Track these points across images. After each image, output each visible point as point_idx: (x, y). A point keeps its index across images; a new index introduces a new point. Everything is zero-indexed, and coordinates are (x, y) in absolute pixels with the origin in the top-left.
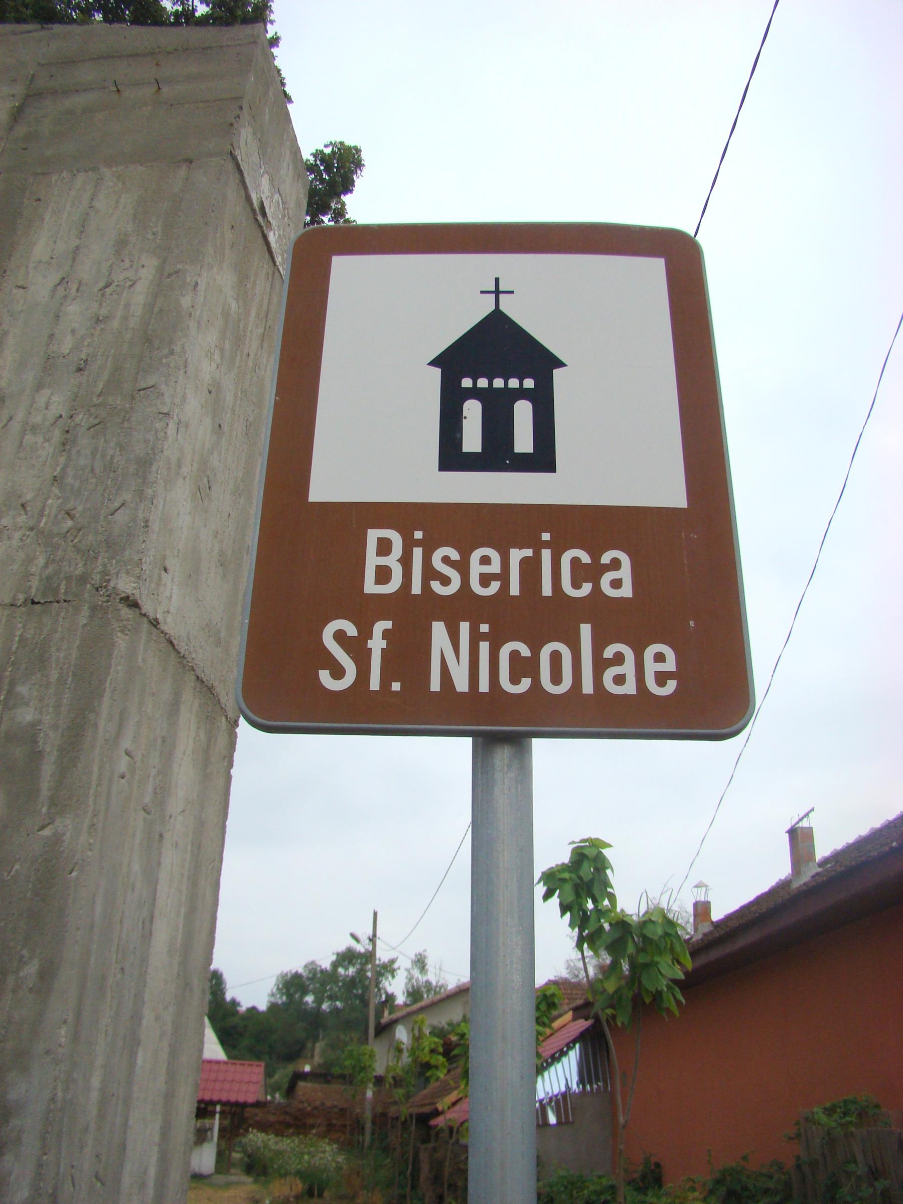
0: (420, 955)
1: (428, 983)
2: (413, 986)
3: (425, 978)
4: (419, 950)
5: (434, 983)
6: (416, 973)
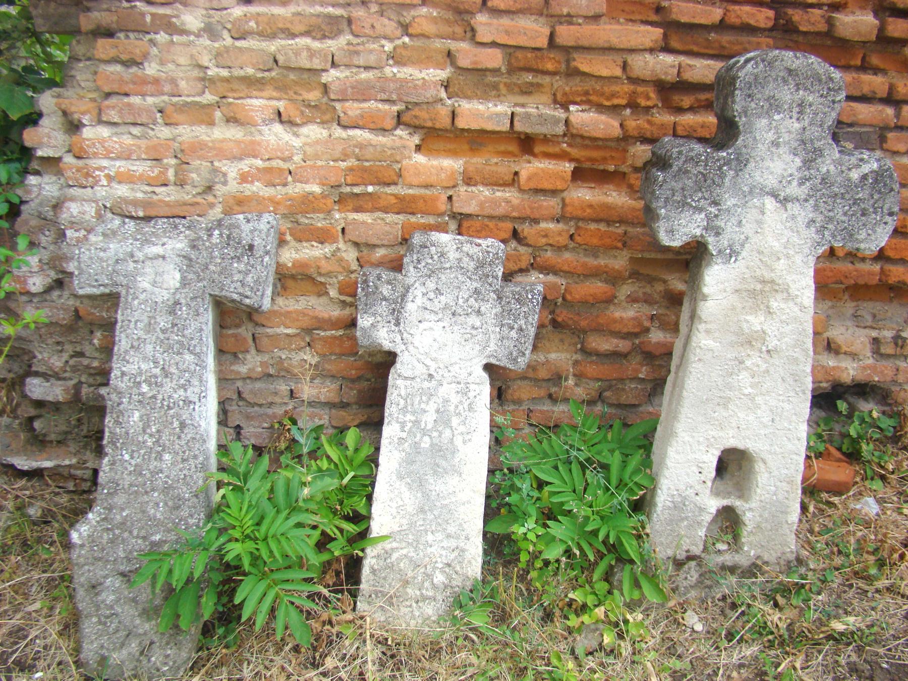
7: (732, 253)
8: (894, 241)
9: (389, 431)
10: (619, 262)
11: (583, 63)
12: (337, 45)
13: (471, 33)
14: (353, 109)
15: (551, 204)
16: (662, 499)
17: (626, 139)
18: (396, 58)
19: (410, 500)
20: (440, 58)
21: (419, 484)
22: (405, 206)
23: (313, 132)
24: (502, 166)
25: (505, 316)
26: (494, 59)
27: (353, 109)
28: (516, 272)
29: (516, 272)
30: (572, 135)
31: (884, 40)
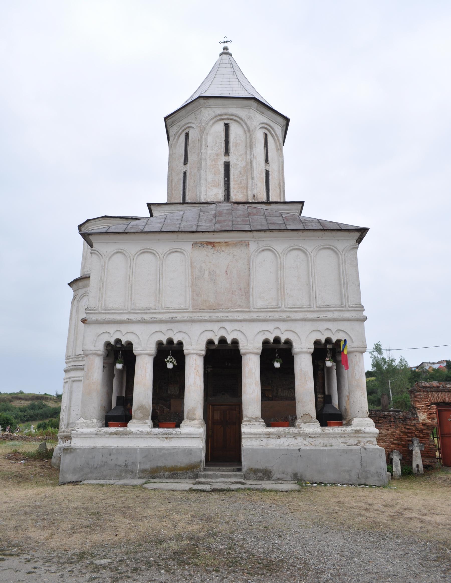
0: (377, 344)
1: (384, 359)
2: (376, 361)
3: (382, 356)
4: (376, 342)
5: (387, 360)
6: (376, 354)
7: (414, 450)
8: (59, 406)
9: (393, 464)
10: (407, 454)
11: (402, 439)
12: (386, 437)
13: (394, 437)
14: (387, 442)
15: (401, 449)
16: (413, 468)
17: (406, 444)
18: (390, 438)
19: (395, 469)
20: (87, 272)
21: (396, 468)
22: (391, 449)
23: (384, 443)
24: (397, 446)
25: (400, 456)
26: (396, 438)
27: (387, 442)
28: (208, 492)
29: (208, 492)
30: (402, 444)
31: (423, 436)
